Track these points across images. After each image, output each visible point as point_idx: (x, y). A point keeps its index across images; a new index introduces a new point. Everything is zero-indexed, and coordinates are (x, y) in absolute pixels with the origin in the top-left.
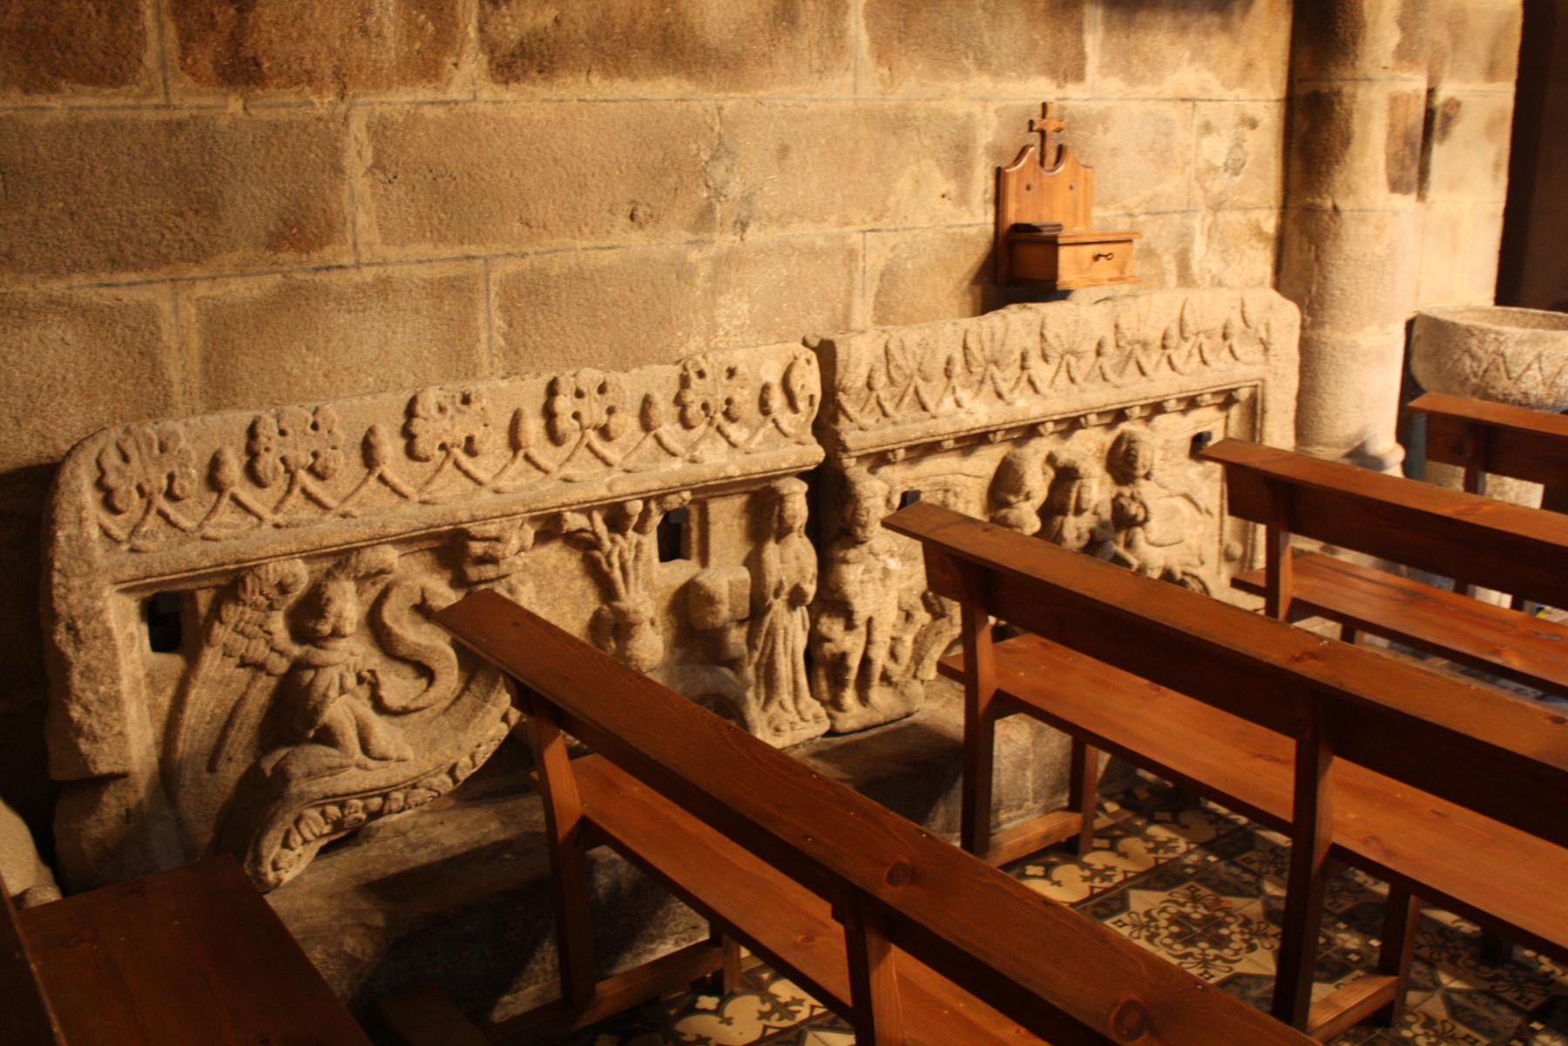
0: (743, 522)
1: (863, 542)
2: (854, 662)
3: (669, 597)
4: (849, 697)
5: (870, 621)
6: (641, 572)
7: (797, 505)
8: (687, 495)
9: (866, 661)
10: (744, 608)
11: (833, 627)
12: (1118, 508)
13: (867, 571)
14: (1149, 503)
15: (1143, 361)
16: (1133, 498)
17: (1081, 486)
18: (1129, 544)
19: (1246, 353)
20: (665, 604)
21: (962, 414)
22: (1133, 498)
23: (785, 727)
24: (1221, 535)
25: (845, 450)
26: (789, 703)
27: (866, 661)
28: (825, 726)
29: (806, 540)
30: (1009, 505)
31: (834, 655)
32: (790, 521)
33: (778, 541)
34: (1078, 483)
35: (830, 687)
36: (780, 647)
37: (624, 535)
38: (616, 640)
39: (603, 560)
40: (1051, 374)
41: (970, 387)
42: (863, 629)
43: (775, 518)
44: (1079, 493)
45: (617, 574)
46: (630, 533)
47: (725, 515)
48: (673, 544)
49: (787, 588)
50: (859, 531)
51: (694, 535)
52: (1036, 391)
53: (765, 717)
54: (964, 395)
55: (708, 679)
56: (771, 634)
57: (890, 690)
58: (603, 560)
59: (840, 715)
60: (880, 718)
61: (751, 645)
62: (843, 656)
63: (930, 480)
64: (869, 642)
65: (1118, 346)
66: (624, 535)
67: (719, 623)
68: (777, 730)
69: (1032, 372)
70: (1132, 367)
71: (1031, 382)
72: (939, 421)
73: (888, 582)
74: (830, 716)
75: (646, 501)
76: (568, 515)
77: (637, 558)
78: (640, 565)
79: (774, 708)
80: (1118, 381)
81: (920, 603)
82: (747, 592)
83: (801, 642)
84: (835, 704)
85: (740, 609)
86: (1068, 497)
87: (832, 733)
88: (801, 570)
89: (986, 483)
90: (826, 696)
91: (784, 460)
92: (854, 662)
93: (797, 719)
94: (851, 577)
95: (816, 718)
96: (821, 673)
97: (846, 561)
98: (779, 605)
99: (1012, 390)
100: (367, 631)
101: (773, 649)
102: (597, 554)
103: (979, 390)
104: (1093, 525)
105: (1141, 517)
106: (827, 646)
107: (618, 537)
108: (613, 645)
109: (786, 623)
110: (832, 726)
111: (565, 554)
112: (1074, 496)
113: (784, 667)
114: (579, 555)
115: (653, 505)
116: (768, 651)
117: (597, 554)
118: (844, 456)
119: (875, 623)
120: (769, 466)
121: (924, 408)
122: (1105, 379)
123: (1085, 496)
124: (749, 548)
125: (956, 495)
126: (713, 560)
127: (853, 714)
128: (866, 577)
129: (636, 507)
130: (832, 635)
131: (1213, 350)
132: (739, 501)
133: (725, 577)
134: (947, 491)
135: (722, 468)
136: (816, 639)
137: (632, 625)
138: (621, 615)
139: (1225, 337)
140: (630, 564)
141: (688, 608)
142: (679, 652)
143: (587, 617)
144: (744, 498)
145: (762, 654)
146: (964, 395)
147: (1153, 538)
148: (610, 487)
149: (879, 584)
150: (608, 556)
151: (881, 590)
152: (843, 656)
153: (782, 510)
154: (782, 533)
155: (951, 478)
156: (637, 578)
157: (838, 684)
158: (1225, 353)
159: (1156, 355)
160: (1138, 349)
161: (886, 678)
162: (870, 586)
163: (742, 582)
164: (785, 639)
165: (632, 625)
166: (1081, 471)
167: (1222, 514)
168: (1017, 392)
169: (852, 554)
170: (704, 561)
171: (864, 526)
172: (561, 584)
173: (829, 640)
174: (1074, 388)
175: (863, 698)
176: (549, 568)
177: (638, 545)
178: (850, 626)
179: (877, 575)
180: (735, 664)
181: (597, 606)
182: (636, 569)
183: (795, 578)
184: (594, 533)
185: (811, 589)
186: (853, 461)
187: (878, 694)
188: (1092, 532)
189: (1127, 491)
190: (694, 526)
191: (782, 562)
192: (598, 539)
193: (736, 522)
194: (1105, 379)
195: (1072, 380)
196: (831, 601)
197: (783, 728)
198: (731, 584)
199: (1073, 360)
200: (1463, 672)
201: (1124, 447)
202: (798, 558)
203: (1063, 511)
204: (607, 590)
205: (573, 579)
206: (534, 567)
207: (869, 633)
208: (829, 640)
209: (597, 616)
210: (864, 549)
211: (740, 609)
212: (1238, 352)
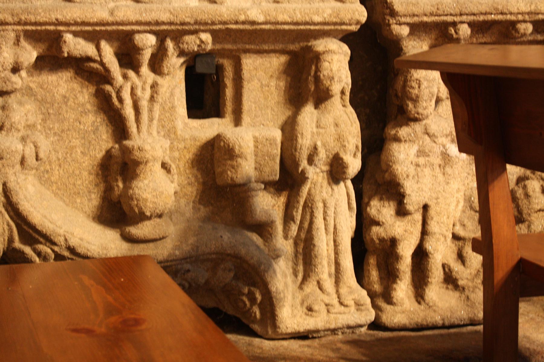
0: (282, 84)
1: (416, 120)
2: (406, 251)
3: (194, 150)
4: (403, 289)
5: (426, 208)
6: (157, 114)
7: (337, 63)
8: (206, 37)
9: (421, 255)
10: (273, 170)
11: (382, 210)
13: (421, 153)
20: (189, 156)
23: (319, 307)
25: (393, 13)
26: (329, 284)
27: (421, 255)
28: (370, 315)
29: (350, 109)
31: (382, 240)
32: (327, 83)
33: (317, 106)
35: (381, 278)
36: (319, 222)
37: (137, 71)
38: (124, 181)
39: (114, 95)
42: (418, 217)
43: (311, 79)
45: (129, 112)
46: (145, 69)
47: (261, 73)
48: (205, 94)
49: (323, 155)
50: (411, 105)
51: (229, 92)
53: (299, 296)
55: (226, 238)
56: (309, 206)
57: (457, 294)
58: (114, 95)
59: (388, 308)
60: (437, 319)
61: (288, 218)
62: (393, 242)
64: (424, 233)
66: (137, 71)
67: (239, 178)
68: (310, 309)
73: (448, 170)
74: (375, 306)
75: (161, 37)
76: (68, 37)
77: (152, 99)
78: (157, 108)
79: (311, 287)
82: (277, 151)
83: (347, 225)
84: (383, 296)
85: (267, 170)
87: (376, 325)
88: (340, 138)
90: (377, 287)
91: (317, 13)
92: (406, 251)
93: (335, 301)
94: (402, 157)
95: (358, 305)
96: (372, 261)
97: (397, 140)
98: (316, 174)
100: (315, 329)
101: (311, 223)
102: (108, 88)
106: (375, 229)
107: (131, 74)
108: (121, 185)
109: (324, 195)
110: (377, 317)
111: (76, 86)
113: (323, 244)
114: (92, 89)
115: (170, 44)
116: (306, 225)
117: (108, 88)
118: (392, 21)
119: (432, 212)
120: (299, 17)
124: (289, 113)
126: (246, 118)
127: (404, 306)
128: (422, 160)
129: (148, 42)
130: (381, 219)
132: (277, 61)
133: (253, 134)
135: (243, 11)
136: (363, 222)
137: (137, 163)
138: (126, 151)
140: (144, 104)
141: (211, 158)
142: (203, 211)
143: (100, 155)
144: (283, 59)
145: (300, 228)
148: (112, 13)
149: (437, 170)
150: (118, 92)
151: (441, 177)
152: (393, 242)
153: (318, 70)
154: (321, 97)
156: (151, 120)
157: (390, 275)
161: (450, 280)
162: (427, 171)
163: (271, 141)
164: (325, 213)
165: (137, 163)
169: (404, 132)
170: (237, 121)
171: (415, 100)
172: (71, 116)
173: (378, 223)
175: (419, 293)
176: (58, 97)
177: (154, 86)
178: (402, 212)
179: (437, 160)
180: (263, 228)
181: (110, 145)
182: (151, 110)
183: (335, 147)
184: (102, 64)
185: (354, 164)
186: (405, 31)
187: (435, 292)
190: (229, 82)
191: (318, 126)
192: (107, 70)
193: (273, 83)
196: (376, 181)
197: (316, 308)
198: (256, 140)
202: (337, 125)
204: (119, 129)
205: (85, 113)
206: (40, 93)
207: (424, 223)
208: (378, 223)
209: (108, 155)
210: (418, 127)
211: (267, 170)
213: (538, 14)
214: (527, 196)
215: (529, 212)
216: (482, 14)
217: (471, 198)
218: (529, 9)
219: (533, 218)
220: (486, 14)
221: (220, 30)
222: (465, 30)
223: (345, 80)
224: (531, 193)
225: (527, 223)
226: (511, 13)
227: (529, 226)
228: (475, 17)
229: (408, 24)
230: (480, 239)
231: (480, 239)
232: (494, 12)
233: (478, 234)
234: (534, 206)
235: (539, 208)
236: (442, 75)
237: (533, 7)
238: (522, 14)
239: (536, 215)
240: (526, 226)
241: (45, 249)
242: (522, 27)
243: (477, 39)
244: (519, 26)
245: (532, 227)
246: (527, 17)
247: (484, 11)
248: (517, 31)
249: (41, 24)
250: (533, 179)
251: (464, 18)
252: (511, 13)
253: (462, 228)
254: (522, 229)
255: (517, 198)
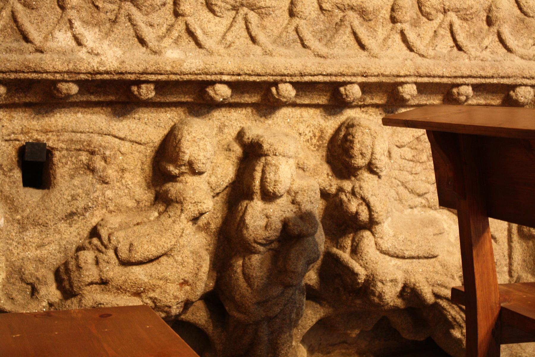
12: (332, 201)
14: (372, 200)
15: (362, 33)
16: (353, 193)
17: (266, 164)
18: (355, 251)
19: (524, 46)
21: (82, 53)
22: (353, 193)
24: (510, 264)
30: (173, 178)
34: (263, 159)
40: (222, 29)
41: (98, 24)
44: (263, 172)
52: (199, 44)
54: (90, 37)
63: (66, 136)
65: (321, 8)
69: (191, 20)
70: (345, 37)
71: (191, 33)
72: (46, 57)
80: (324, 51)
81: (51, 277)
86: (253, 179)
89: (149, 152)
99: (161, 38)
103: (111, 30)
104: (289, 214)
105: (364, 216)
112: (258, 175)
121: (26, 39)
122: (304, 46)
123: (271, 176)
125: (105, 159)
131: (472, 36)
134: (93, 153)
139: (489, 22)
146: (90, 37)
147: (386, 245)
155: (97, 139)
158: (491, 40)
159: (383, 29)
160: (353, 17)
166: (265, 146)
167: (510, 240)
168: (167, 42)
174: (257, 49)
188: (285, 223)
189: (347, 185)
194: (304, 46)
195: (253, 40)
199: (253, 17)
200: (55, 178)
201: (343, 133)
203: (249, 196)
212: (511, 42)
213: (79, 73)
214: (79, 267)
215: (80, 285)
216: (12, 71)
217: (21, 269)
218: (67, 68)
219: (85, 292)
220: (16, 72)
221: (87, 80)
222: (355, 91)
223: (420, 134)
224: (83, 265)
225: (79, 297)
226: (47, 72)
227: (81, 300)
228: (4, 75)
229: (290, 82)
230: (463, 289)
231: (463, 289)
232: (26, 70)
233: (458, 283)
234: (84, 279)
235: (89, 281)
236: (428, 133)
237: (71, 66)
238: (60, 72)
239: (88, 288)
240: (78, 300)
241: (83, 284)
242: (63, 87)
243: (18, 98)
244: (59, 85)
245: (83, 301)
246: (66, 76)
247: (13, 69)
248: (58, 90)
249: (485, 77)
250: (88, 249)
251: (468, 81)
252: (47, 72)
253: (10, 302)
254: (73, 305)
255: (69, 269)
